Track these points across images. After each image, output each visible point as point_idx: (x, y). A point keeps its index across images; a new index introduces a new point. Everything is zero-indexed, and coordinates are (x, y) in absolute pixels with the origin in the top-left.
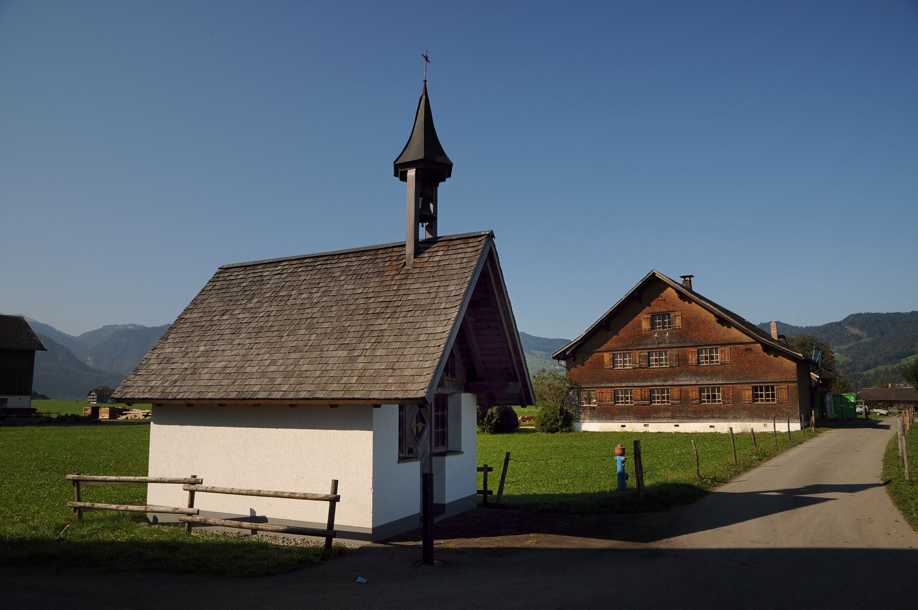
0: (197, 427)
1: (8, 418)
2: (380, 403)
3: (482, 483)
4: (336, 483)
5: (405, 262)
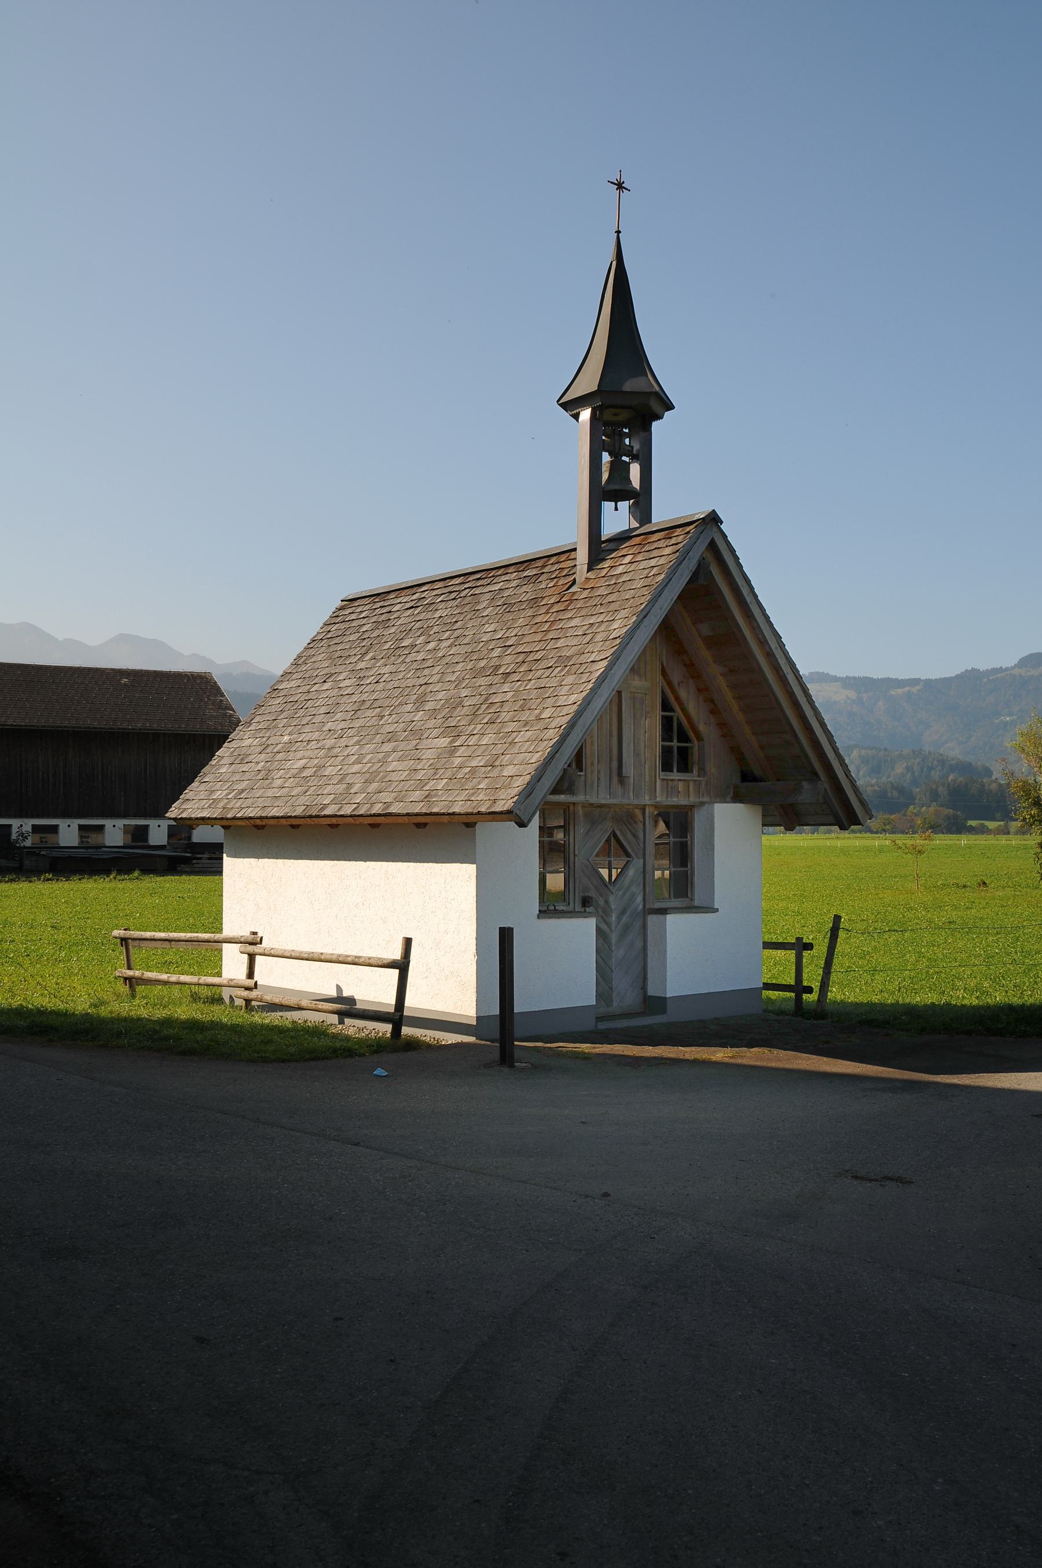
0: (275, 860)
1: (194, 861)
2: (475, 821)
3: (793, 975)
4: (408, 942)
5: (575, 579)
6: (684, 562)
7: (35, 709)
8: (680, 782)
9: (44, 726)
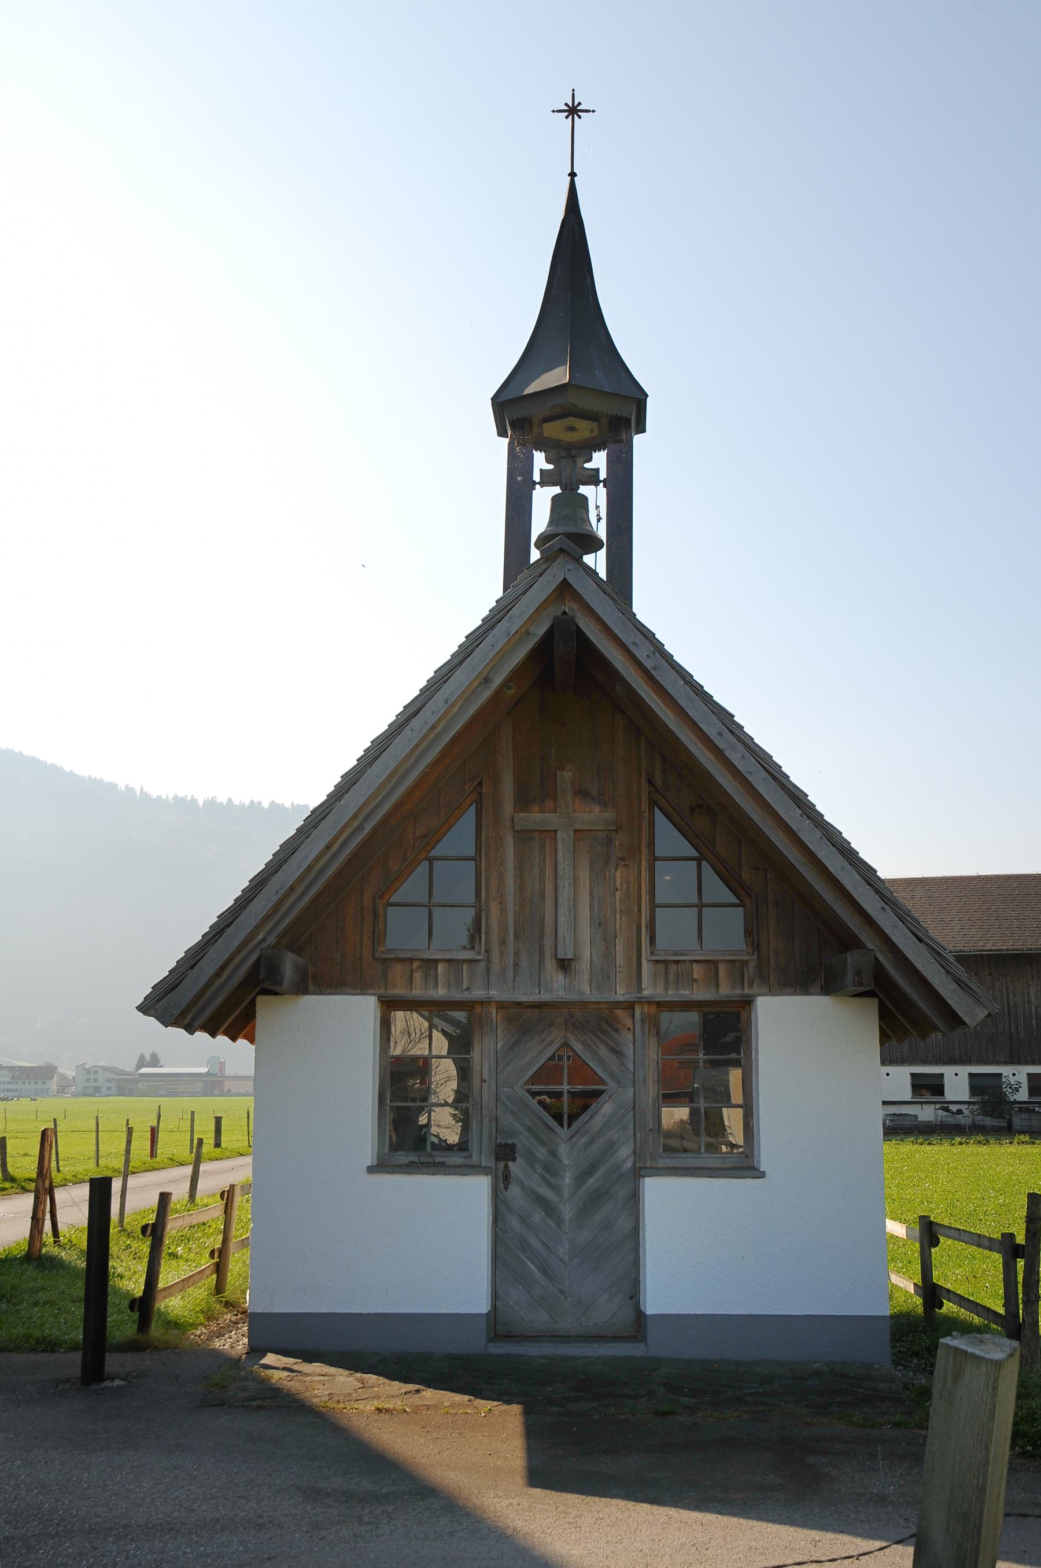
6: (499, 625)
7: (1024, 929)
8: (694, 965)
9: (1031, 949)
